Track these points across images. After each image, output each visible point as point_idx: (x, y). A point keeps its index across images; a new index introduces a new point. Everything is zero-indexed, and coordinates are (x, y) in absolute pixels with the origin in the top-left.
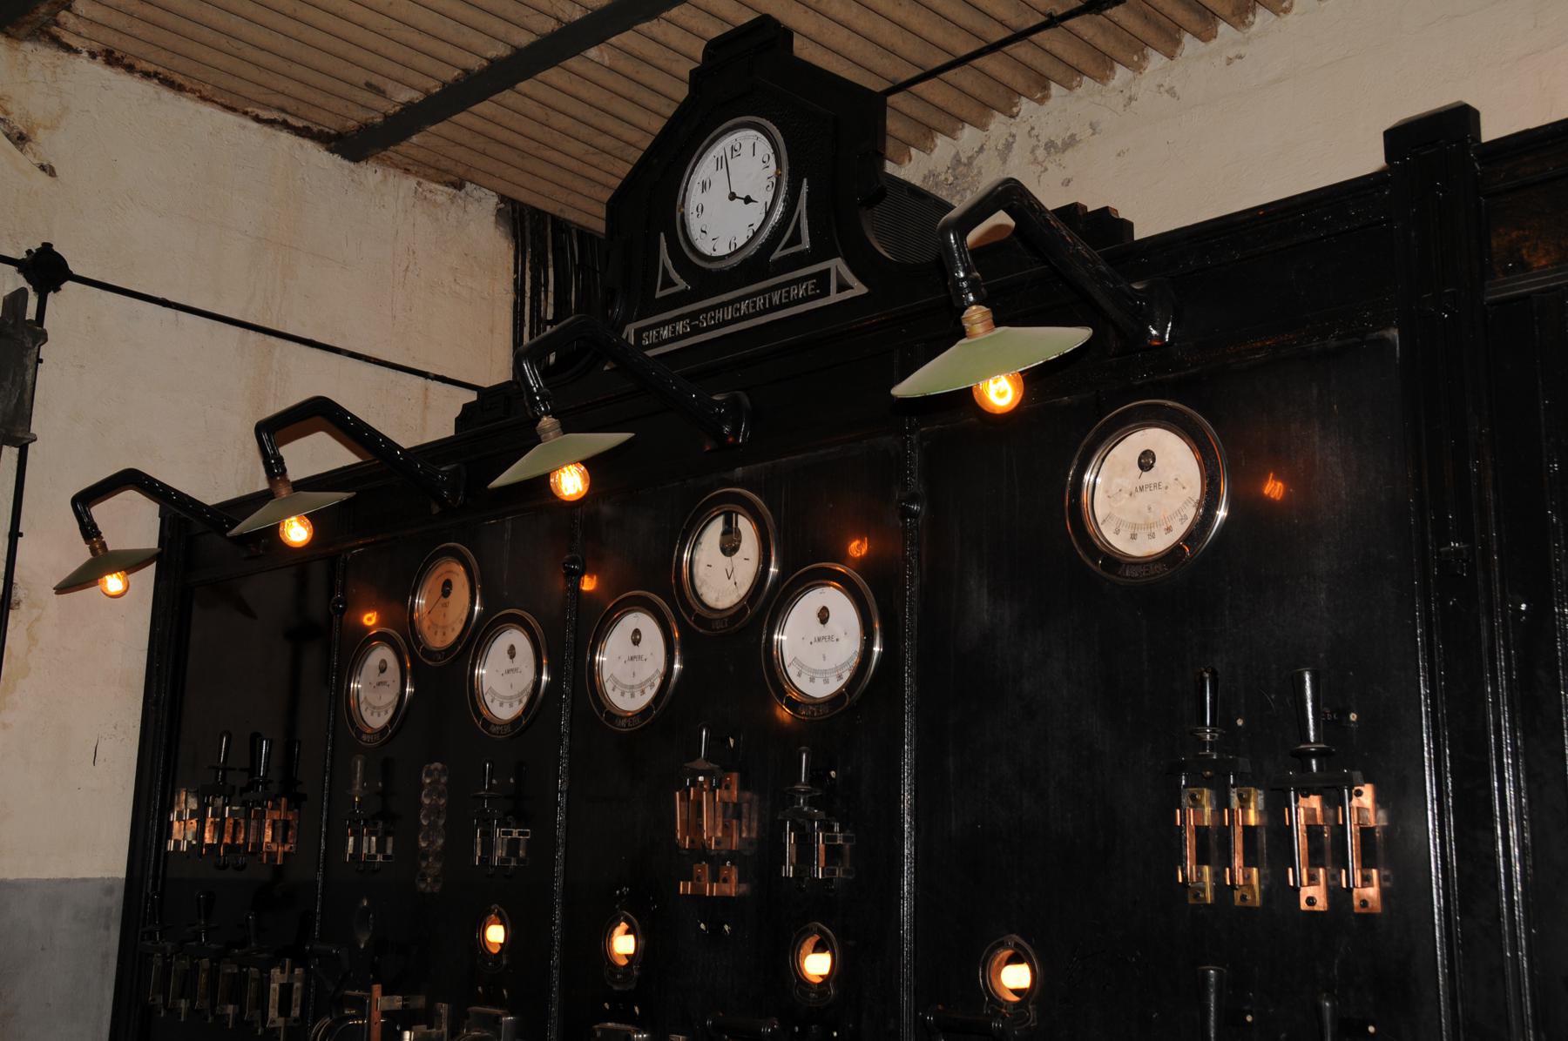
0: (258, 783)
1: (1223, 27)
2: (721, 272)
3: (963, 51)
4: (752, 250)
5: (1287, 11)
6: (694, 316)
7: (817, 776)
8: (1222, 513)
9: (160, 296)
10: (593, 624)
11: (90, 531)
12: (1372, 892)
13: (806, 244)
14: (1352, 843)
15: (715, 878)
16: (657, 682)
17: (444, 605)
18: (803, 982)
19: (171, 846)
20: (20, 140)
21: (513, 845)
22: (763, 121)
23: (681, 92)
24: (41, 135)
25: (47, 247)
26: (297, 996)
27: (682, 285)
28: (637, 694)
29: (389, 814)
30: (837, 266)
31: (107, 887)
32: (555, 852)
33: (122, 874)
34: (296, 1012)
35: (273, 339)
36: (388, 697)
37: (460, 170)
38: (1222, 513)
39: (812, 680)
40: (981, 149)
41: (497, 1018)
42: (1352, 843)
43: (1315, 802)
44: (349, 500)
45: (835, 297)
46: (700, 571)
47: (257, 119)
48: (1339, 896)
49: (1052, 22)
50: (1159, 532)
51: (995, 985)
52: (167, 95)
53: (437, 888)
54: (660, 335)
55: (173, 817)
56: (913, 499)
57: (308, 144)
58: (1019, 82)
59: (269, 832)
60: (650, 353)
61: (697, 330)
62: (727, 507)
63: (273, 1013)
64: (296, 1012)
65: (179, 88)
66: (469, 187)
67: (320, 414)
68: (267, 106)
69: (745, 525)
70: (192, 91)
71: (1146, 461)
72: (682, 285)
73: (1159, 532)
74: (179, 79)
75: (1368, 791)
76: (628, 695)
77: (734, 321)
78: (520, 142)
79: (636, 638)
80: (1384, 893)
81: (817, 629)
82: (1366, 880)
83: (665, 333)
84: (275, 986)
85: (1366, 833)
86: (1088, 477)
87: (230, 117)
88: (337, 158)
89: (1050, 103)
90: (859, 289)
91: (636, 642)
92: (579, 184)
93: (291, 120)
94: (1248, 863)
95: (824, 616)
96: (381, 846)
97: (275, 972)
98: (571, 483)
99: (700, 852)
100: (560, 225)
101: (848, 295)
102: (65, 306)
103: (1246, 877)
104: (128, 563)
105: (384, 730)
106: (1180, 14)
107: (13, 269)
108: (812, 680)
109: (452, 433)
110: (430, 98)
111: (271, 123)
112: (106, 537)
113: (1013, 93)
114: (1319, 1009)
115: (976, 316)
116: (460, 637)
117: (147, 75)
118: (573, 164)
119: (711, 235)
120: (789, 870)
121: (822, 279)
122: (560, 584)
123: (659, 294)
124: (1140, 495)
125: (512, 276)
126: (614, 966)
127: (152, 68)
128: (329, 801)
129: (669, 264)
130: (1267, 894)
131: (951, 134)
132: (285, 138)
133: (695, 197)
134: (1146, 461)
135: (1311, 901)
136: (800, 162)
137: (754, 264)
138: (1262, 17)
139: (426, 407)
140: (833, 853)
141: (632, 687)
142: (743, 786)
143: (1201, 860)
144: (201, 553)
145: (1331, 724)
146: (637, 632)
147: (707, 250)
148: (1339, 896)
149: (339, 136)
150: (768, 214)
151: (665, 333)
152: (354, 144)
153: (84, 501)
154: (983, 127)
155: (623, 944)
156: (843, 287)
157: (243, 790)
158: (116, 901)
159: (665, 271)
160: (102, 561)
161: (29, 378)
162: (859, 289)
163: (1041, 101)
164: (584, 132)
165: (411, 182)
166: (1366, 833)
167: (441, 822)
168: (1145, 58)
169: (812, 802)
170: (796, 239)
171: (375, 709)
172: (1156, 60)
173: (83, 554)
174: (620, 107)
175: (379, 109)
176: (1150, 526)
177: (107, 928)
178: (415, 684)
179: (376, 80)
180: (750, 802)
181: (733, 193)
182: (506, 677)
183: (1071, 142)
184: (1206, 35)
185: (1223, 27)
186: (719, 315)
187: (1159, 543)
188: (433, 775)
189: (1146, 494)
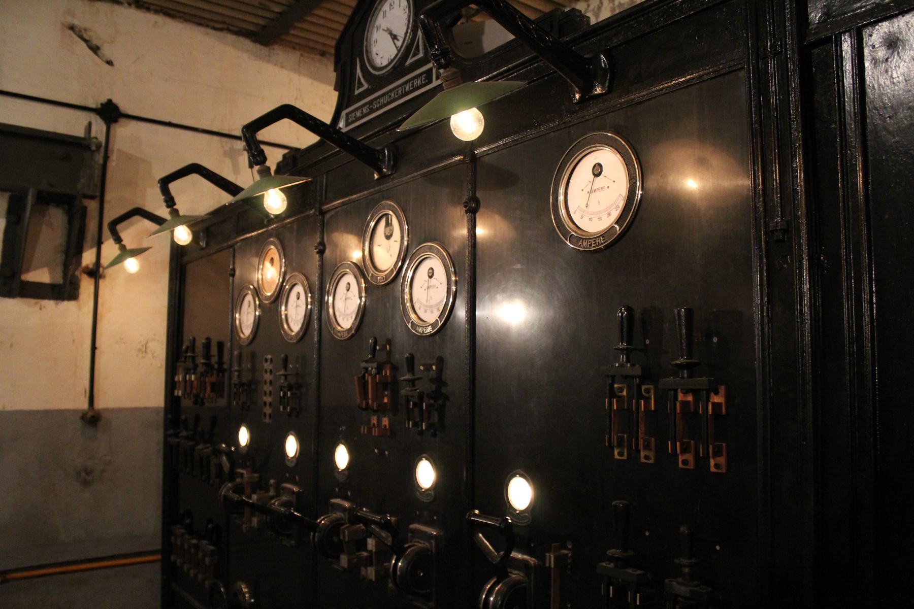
9: (167, 120)
18: (529, 475)
25: (110, 101)
31: (155, 410)
32: (754, 339)
59: (209, 389)
61: (372, 111)
68: (216, 22)
74: (172, 12)
77: (389, 103)
83: (358, 114)
88: (258, 46)
93: (232, 28)
111: (221, 30)
119: (380, 55)
141: (431, 306)
146: (349, 284)
151: (358, 114)
158: (161, 417)
159: (359, 79)
165: (298, 53)
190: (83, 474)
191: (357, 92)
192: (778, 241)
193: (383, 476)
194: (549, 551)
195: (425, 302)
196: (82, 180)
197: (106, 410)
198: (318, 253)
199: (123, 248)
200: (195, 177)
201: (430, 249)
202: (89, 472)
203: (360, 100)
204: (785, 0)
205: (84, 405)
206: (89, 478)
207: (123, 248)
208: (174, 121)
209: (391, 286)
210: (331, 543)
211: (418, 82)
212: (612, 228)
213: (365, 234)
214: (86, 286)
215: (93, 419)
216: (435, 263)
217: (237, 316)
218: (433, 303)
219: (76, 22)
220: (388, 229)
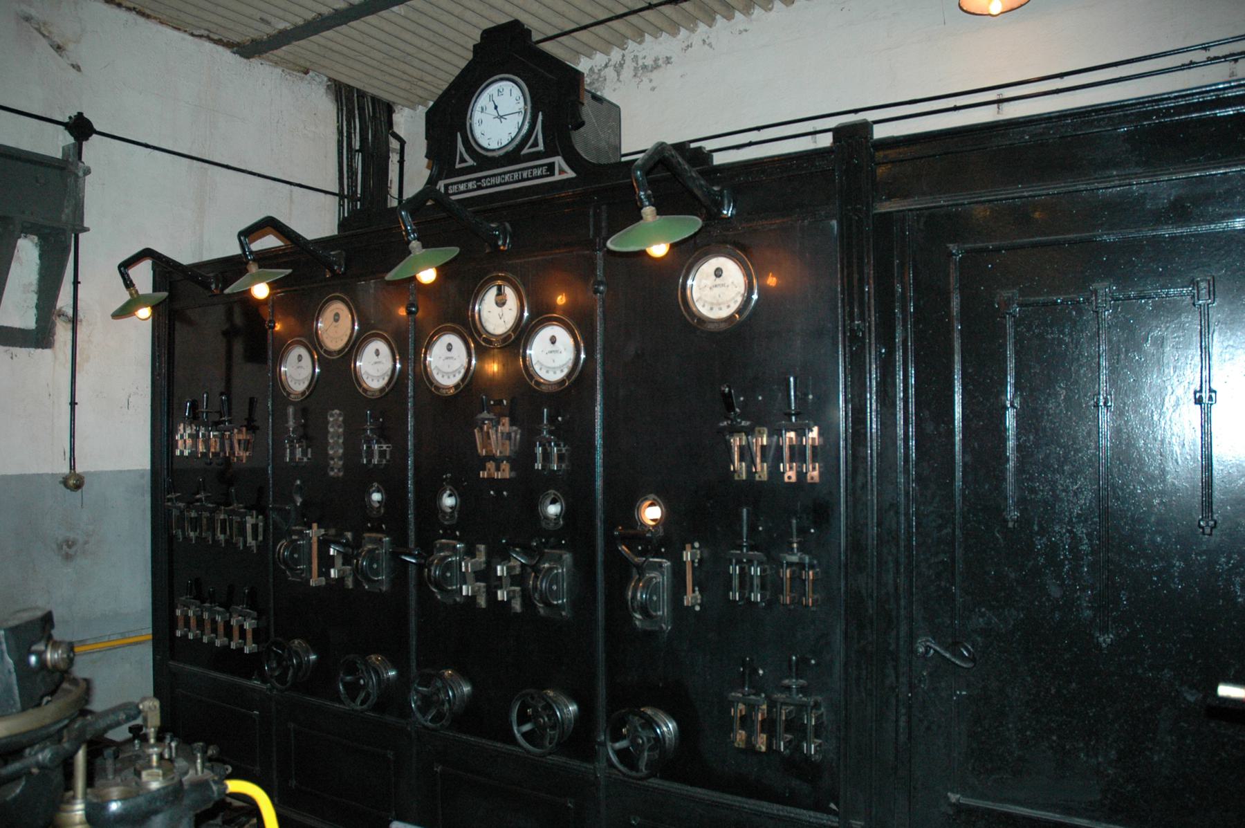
1: (737, 14)
2: (493, 158)
3: (602, 17)
4: (510, 148)
5: (770, 10)
6: (479, 180)
7: (552, 419)
8: (755, 297)
10: (424, 342)
11: (129, 284)
12: (816, 473)
13: (541, 147)
14: (809, 453)
15: (498, 469)
16: (463, 371)
17: (335, 325)
19: (178, 453)
20: (59, 48)
21: (382, 454)
22: (516, 78)
23: (470, 56)
24: (71, 47)
25: (80, 114)
26: (261, 530)
27: (470, 162)
29: (312, 434)
30: (558, 160)
31: (141, 474)
33: (148, 467)
34: (260, 538)
35: (207, 165)
37: (308, 64)
38: (755, 297)
40: (606, 66)
41: (381, 539)
42: (809, 453)
43: (792, 434)
44: (290, 275)
45: (557, 177)
46: (485, 314)
47: (192, 35)
48: (801, 475)
49: (650, 7)
50: (724, 307)
52: (141, 20)
53: (341, 474)
54: (460, 189)
55: (178, 437)
56: (600, 283)
57: (220, 48)
58: (628, 33)
59: (236, 446)
60: (453, 198)
62: (499, 282)
63: (249, 539)
64: (260, 538)
65: (148, 17)
66: (311, 73)
67: (270, 224)
69: (509, 292)
70: (155, 18)
71: (718, 273)
72: (470, 162)
73: (724, 307)
74: (148, 12)
75: (816, 429)
78: (345, 51)
79: (449, 347)
80: (821, 474)
81: (550, 347)
82: (814, 469)
83: (462, 187)
84: (249, 526)
85: (814, 447)
86: (689, 282)
87: (176, 33)
89: (644, 45)
90: (571, 174)
91: (449, 350)
92: (377, 74)
93: (212, 36)
94: (762, 461)
95: (553, 340)
96: (304, 453)
97: (248, 518)
99: (491, 457)
100: (362, 94)
101: (564, 176)
102: (93, 149)
103: (762, 470)
105: (303, 393)
106: (717, 7)
107: (62, 128)
109: (336, 233)
110: (297, 28)
111: (201, 36)
112: (137, 286)
113: (625, 37)
114: (790, 523)
115: (648, 211)
116: (347, 344)
117: (129, 9)
118: (375, 63)
120: (538, 466)
121: (551, 167)
123: (458, 166)
124: (715, 290)
125: (336, 125)
126: (444, 512)
127: (132, 5)
129: (463, 150)
130: (770, 473)
131: (589, 57)
132: (208, 45)
133: (477, 115)
134: (718, 273)
135: (789, 478)
136: (538, 102)
137: (512, 156)
138: (757, 12)
139: (291, 201)
140: (561, 458)
142: (512, 424)
143: (741, 459)
145: (801, 399)
146: (450, 345)
147: (485, 145)
148: (801, 475)
149: (238, 45)
150: (520, 129)
152: (249, 50)
153: (125, 266)
154: (607, 54)
155: (448, 501)
156: (562, 171)
162: (571, 174)
163: (640, 43)
164: (383, 47)
165: (279, 70)
166: (814, 447)
167: (341, 441)
168: (696, 25)
169: (550, 432)
170: (535, 144)
171: (298, 381)
172: (702, 27)
173: (125, 296)
174: (407, 36)
175: (265, 31)
176: (719, 304)
178: (320, 367)
179: (266, 16)
180: (516, 432)
181: (500, 115)
182: (375, 366)
183: (656, 67)
184: (729, 17)
185: (737, 14)
186: (493, 181)
187: (724, 313)
188: (335, 419)
189: (717, 289)
191: (458, 166)
194: (501, 588)
196: (67, 211)
197: (98, 475)
202: (70, 544)
203: (459, 175)
205: (65, 470)
206: (71, 552)
208: (322, 195)
211: (538, 172)
214: (62, 333)
215: (74, 482)
218: (557, 364)
219: (33, 12)
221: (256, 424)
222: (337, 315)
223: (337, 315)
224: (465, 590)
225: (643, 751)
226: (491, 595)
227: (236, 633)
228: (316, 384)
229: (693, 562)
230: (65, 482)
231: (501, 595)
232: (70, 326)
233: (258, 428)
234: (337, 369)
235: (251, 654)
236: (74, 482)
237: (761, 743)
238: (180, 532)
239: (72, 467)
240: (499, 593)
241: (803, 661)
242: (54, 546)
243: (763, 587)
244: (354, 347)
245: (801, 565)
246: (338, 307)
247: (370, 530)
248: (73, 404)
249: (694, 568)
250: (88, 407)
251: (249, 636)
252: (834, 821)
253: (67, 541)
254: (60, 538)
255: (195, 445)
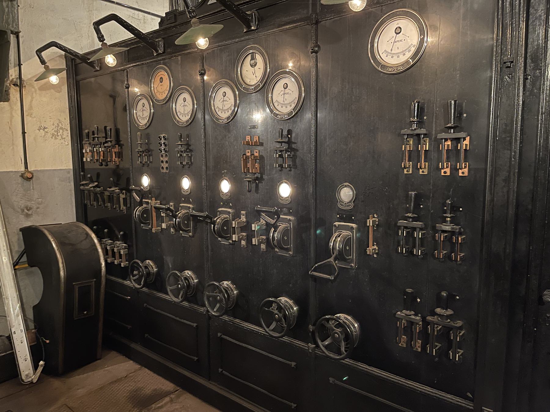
0: (211, 220)
18: (150, 176)
28: (226, 112)
31: (68, 171)
34: (128, 205)
36: (147, 114)
39: (282, 107)
51: (292, 187)
59: (114, 155)
64: (128, 205)
69: (259, 58)
76: (223, 113)
94: (409, 161)
98: (202, 43)
104: (57, 72)
108: (282, 107)
122: (199, 77)
128: (538, 132)
134: (398, 31)
135: (445, 172)
144: (78, 66)
153: (39, 52)
157: (104, 143)
160: (48, 71)
161: (16, 11)
177: (70, 182)
182: (184, 108)
190: (26, 210)
192: (507, 67)
193: (166, 187)
195: (282, 102)
198: (200, 75)
199: (47, 68)
200: (113, 22)
201: (182, 89)
204: (308, 1)
206: (30, 213)
207: (47, 68)
209: (168, 104)
210: (225, 230)
212: (407, 62)
213: (146, 80)
214: (14, 93)
215: (27, 177)
216: (186, 95)
217: (135, 111)
220: (253, 61)
221: (122, 142)
222: (161, 78)
223: (161, 78)
224: (235, 237)
225: (341, 341)
226: (249, 241)
227: (117, 256)
228: (152, 119)
229: (373, 226)
230: (22, 176)
231: (255, 241)
232: (18, 89)
233: (123, 145)
234: (162, 110)
235: (125, 267)
236: (27, 177)
237: (418, 345)
238: (89, 201)
239: (26, 167)
240: (253, 239)
241: (451, 297)
242: (19, 210)
243: (422, 245)
244: (171, 97)
245: (452, 233)
246: (163, 74)
247: (184, 202)
248: (24, 133)
249: (374, 231)
250: (36, 135)
251: (124, 257)
252: (470, 405)
253: (27, 208)
254: (23, 206)
255: (93, 156)
